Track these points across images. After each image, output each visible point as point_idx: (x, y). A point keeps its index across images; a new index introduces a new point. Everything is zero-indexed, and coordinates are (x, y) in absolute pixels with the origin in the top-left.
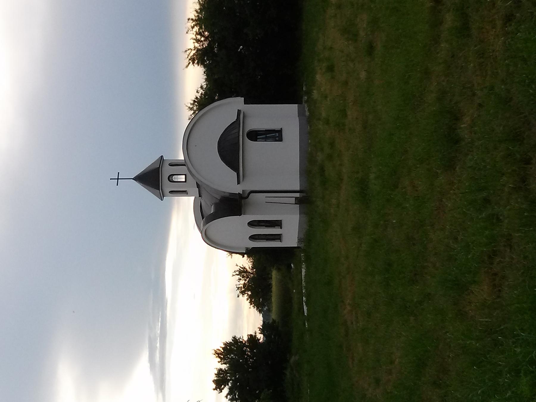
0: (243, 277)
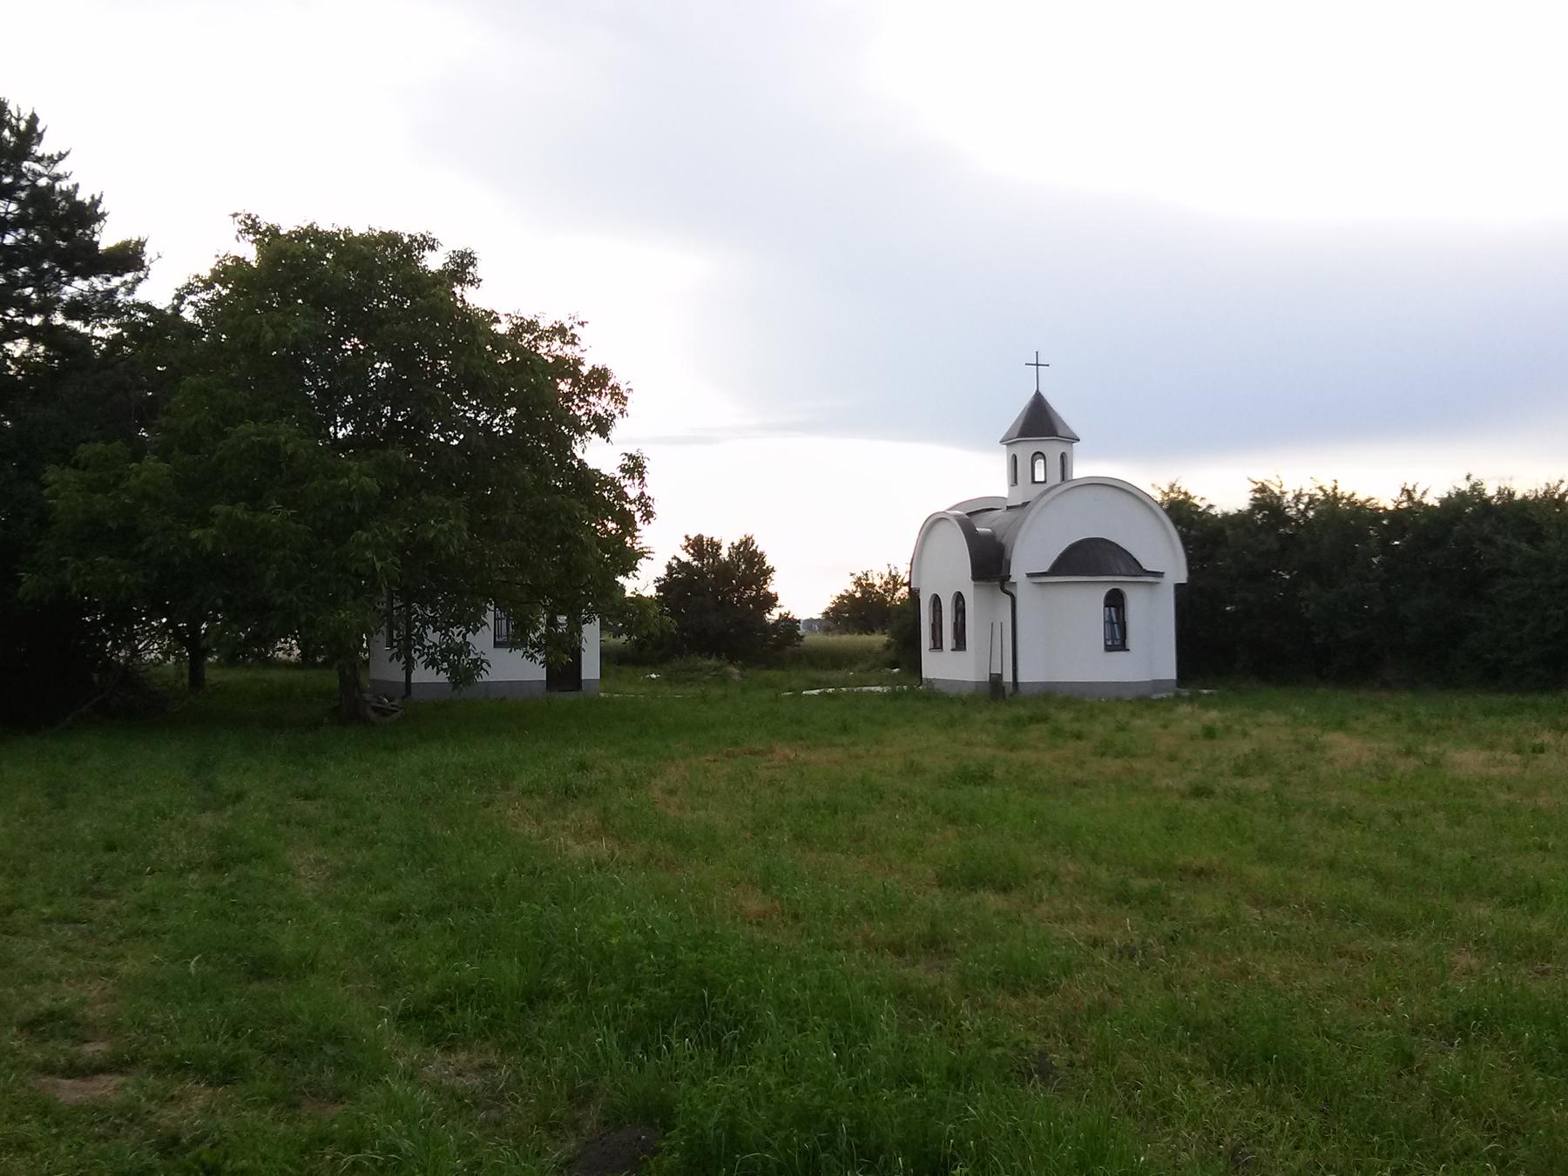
0: (887, 583)
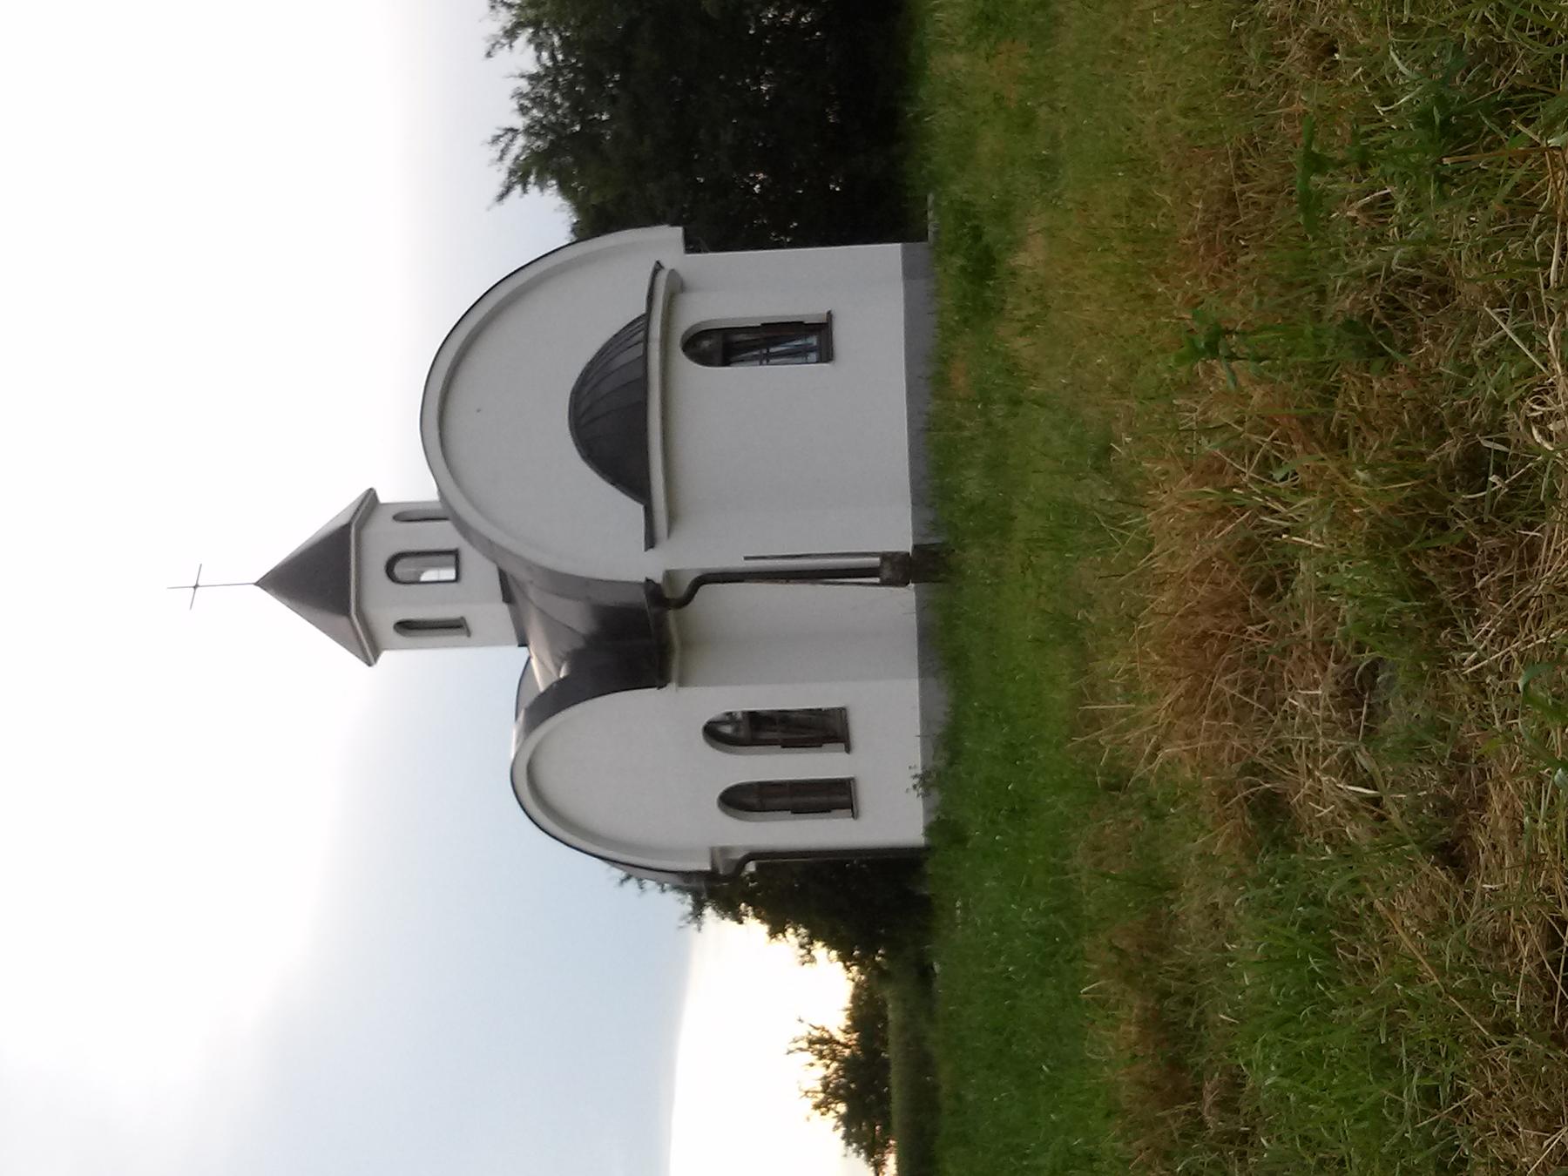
0: (821, 1056)
